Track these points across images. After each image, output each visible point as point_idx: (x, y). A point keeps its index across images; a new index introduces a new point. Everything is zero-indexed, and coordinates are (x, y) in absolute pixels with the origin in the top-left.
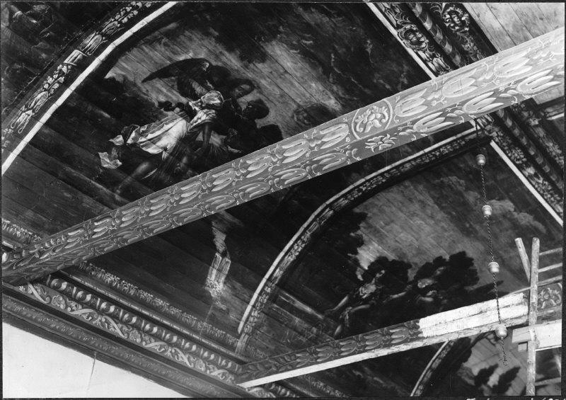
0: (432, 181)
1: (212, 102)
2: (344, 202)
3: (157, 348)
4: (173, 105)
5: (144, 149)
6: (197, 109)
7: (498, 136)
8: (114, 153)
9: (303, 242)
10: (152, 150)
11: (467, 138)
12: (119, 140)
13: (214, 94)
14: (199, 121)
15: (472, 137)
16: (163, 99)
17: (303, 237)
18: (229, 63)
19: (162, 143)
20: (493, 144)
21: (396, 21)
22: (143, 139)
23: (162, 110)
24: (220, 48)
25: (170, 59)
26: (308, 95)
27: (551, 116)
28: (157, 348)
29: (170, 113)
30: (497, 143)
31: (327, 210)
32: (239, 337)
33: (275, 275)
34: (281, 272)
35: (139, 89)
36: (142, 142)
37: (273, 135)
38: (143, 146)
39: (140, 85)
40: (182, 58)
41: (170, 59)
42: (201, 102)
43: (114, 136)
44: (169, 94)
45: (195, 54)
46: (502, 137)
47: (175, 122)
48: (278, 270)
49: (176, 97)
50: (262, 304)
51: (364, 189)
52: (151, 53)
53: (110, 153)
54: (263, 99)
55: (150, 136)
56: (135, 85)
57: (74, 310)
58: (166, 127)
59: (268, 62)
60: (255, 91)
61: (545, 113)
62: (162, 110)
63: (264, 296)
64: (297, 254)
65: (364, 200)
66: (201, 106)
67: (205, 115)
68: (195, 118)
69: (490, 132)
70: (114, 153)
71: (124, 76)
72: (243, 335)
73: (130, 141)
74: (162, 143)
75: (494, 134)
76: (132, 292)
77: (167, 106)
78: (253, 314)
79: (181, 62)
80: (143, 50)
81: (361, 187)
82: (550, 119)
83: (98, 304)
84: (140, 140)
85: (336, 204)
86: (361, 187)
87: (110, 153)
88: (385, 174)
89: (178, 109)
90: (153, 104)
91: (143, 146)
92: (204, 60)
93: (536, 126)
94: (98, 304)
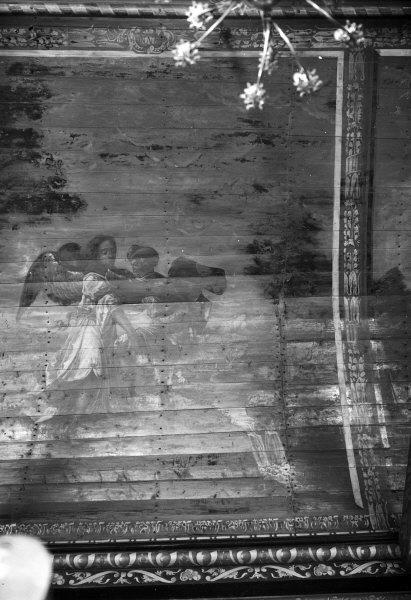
1: (96, 289)
3: (369, 571)
5: (69, 380)
9: (356, 356)
10: (79, 376)
13: (90, 277)
14: (105, 317)
19: (85, 363)
20: (384, 52)
21: (116, 42)
22: (62, 372)
28: (369, 571)
30: (384, 48)
36: (62, 376)
37: (41, 281)
38: (67, 378)
42: (87, 297)
55: (67, 364)
57: (349, 571)
58: (76, 346)
64: (363, 374)
72: (371, 508)
74: (85, 363)
81: (345, 244)
83: (351, 553)
91: (67, 378)
94: (351, 553)
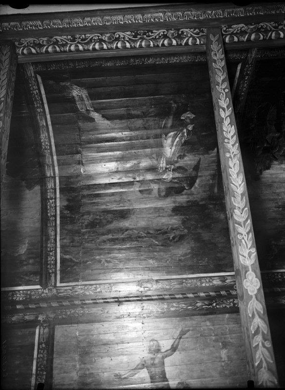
0: (28, 238)
2: (50, 185)
4: (179, 160)
6: (168, 166)
7: (43, 293)
8: (188, 121)
11: (53, 275)
12: (190, 128)
15: (53, 278)
16: (186, 158)
17: (49, 151)
18: (182, 197)
20: (38, 287)
23: (182, 154)
24: (191, 198)
25: (200, 176)
26: (139, 216)
27: (40, 329)
29: (178, 155)
30: (37, 289)
31: (52, 174)
32: (35, 73)
33: (44, 121)
34: (41, 125)
35: (199, 155)
38: (177, 133)
39: (201, 156)
40: (198, 181)
41: (200, 176)
43: (194, 128)
44: (185, 163)
45: (196, 188)
46: (41, 295)
47: (172, 154)
48: (45, 124)
49: (181, 163)
50: (36, 100)
51: (50, 201)
52: (209, 172)
53: (190, 119)
54: (150, 196)
56: (202, 154)
58: (174, 148)
59: (170, 213)
60: (157, 196)
61: (45, 327)
62: (182, 154)
63: (39, 105)
65: (42, 196)
66: (168, 169)
67: (161, 166)
68: (165, 162)
69: (51, 290)
70: (188, 121)
71: (210, 154)
73: (185, 130)
74: (169, 141)
75: (46, 291)
76: (132, 60)
77: (181, 157)
78: (37, 91)
79: (196, 179)
80: (214, 170)
81: (53, 200)
82: (38, 327)
84: (180, 134)
85: (53, 181)
86: (53, 200)
87: (190, 119)
88: (54, 218)
89: (176, 159)
90: (188, 153)
92: (191, 188)
93: (37, 317)
